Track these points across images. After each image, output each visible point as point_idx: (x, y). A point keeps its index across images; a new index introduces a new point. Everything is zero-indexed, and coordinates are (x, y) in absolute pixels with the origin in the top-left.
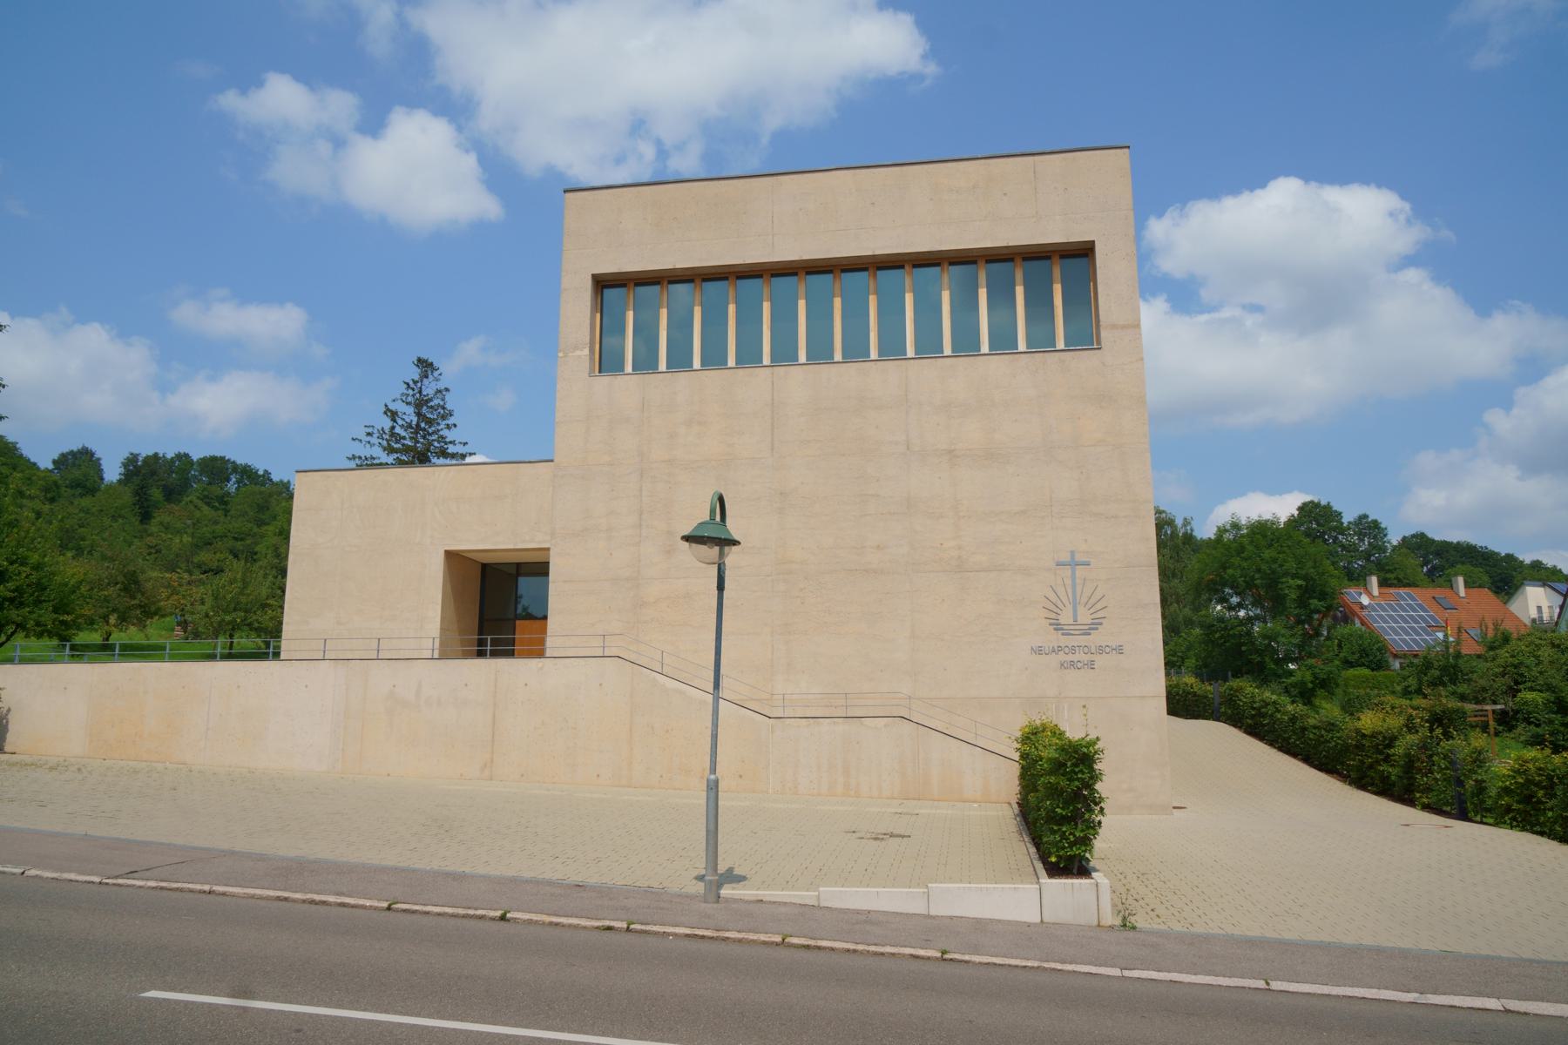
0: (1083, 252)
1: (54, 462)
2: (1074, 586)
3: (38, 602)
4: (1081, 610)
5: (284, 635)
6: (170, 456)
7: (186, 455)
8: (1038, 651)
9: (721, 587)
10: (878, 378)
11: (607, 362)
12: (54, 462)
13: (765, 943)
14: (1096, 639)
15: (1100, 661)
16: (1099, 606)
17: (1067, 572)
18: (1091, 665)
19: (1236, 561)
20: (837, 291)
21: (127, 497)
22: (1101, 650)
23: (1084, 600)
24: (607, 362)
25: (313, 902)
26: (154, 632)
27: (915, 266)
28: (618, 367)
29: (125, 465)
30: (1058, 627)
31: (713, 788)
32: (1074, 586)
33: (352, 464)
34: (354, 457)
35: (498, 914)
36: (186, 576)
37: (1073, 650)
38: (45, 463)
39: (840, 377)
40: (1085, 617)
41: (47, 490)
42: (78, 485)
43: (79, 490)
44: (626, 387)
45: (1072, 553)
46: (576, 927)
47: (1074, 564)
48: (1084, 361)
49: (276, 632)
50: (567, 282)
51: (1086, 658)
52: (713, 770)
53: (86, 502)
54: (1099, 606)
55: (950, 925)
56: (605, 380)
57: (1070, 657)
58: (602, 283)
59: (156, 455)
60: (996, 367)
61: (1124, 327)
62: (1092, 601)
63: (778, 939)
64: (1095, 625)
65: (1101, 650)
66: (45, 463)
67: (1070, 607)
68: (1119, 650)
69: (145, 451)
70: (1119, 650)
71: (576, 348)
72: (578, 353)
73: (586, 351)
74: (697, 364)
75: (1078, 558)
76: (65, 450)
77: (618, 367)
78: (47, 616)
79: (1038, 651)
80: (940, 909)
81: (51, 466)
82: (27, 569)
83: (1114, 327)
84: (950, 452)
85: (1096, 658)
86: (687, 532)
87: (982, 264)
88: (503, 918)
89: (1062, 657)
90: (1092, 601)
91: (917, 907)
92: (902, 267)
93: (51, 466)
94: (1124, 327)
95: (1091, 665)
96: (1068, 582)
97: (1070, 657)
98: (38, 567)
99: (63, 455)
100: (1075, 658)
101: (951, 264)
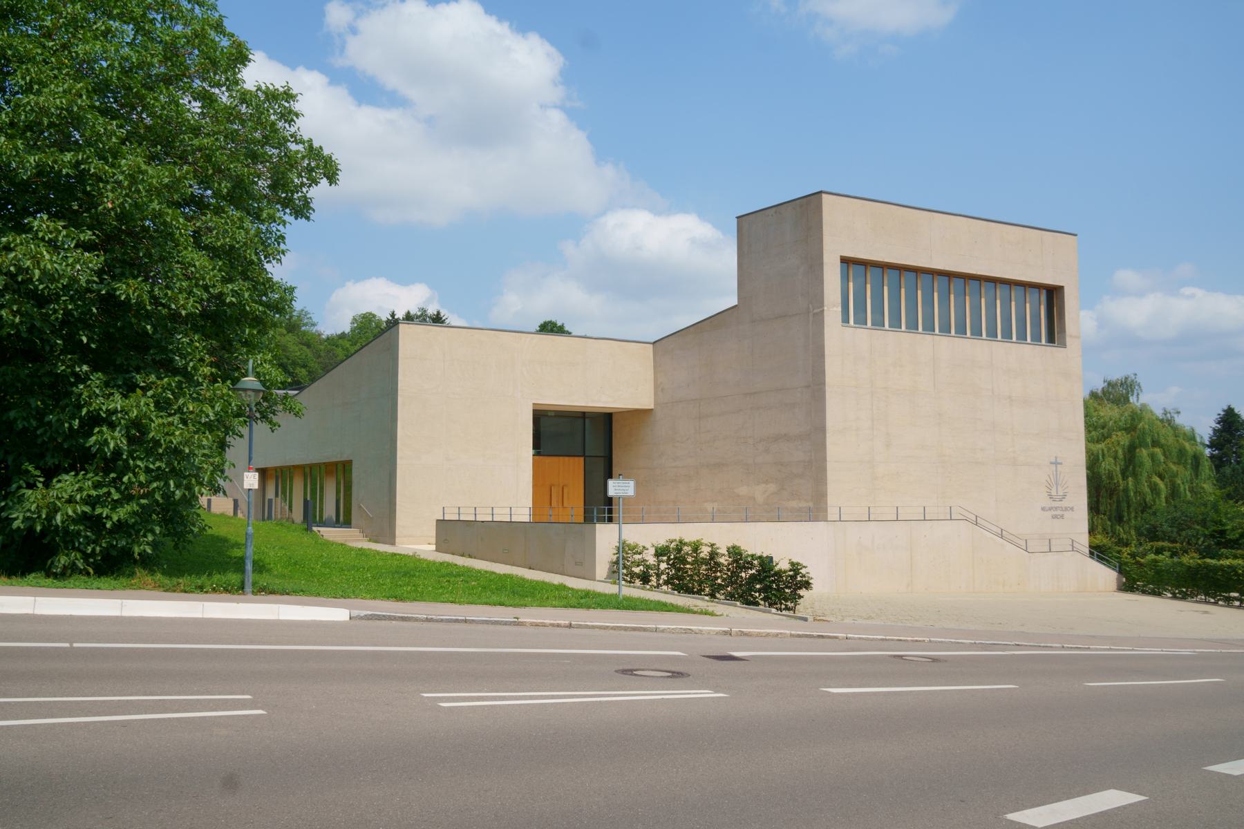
8: (1043, 509)
15: (1067, 514)
17: (1053, 467)
18: (1062, 517)
22: (1066, 509)
30: (1051, 497)
37: (1056, 508)
47: (1056, 463)
49: (816, 468)
58: (1053, 294)
65: (1066, 509)
68: (1072, 509)
70: (1072, 509)
79: (1043, 509)
84: (1010, 397)
95: (1062, 517)
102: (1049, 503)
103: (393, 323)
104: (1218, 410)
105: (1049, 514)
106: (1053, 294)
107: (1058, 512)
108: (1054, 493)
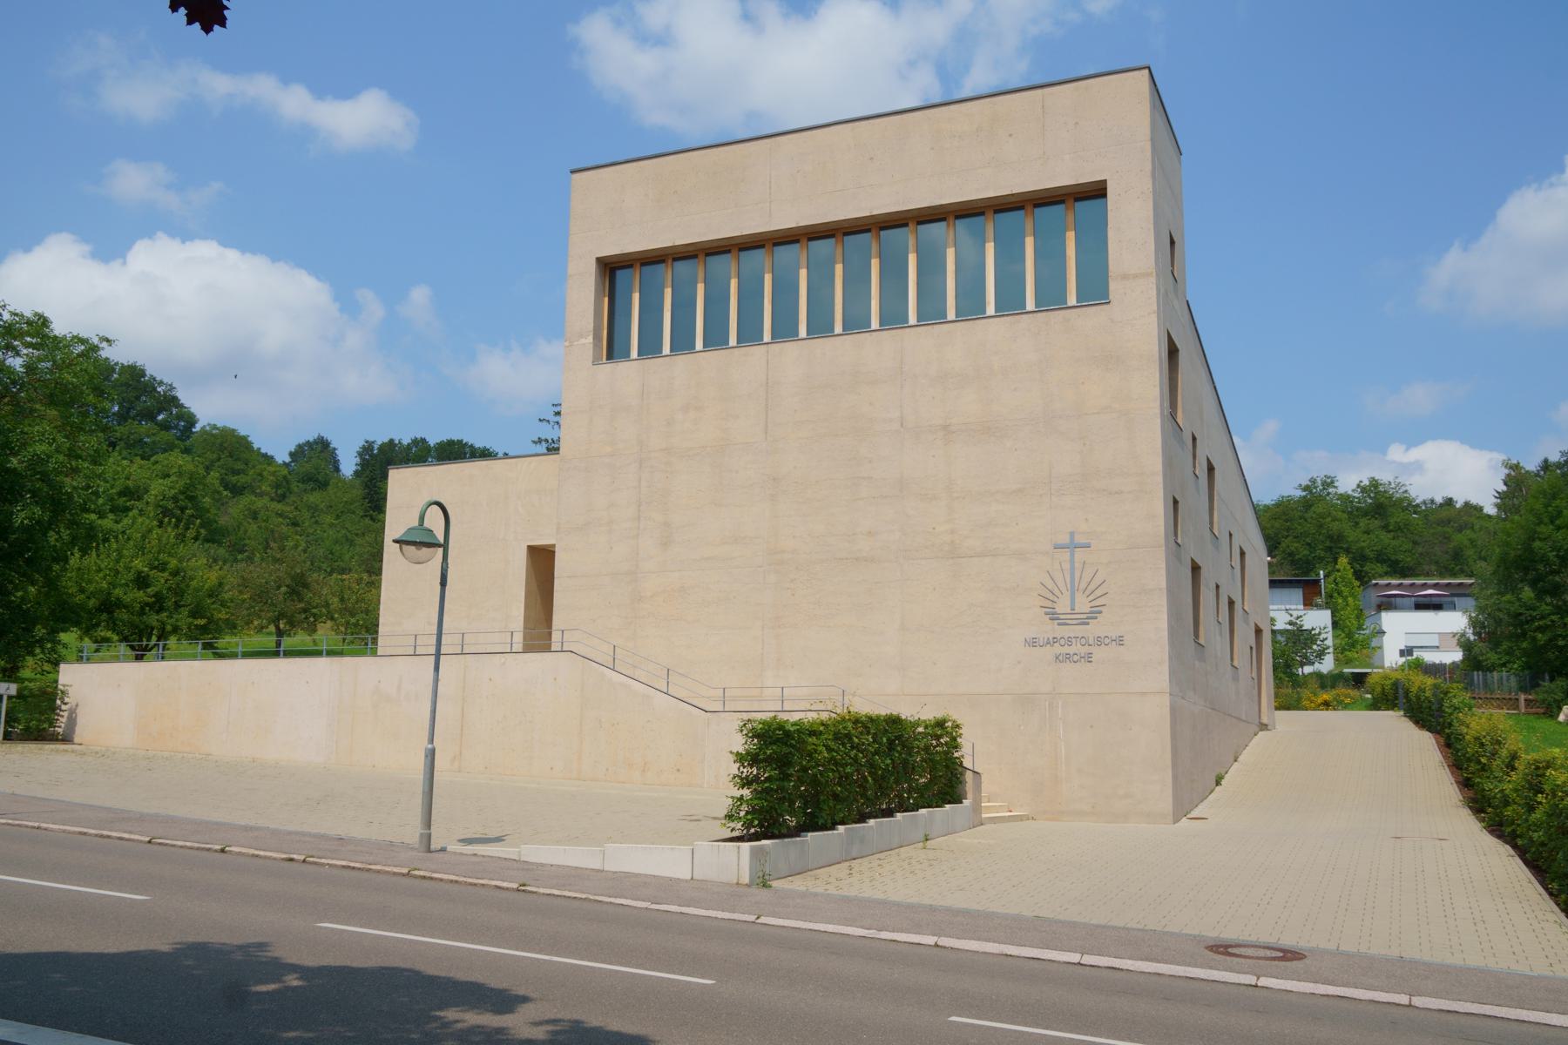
0: (1097, 192)
1: (291, 454)
2: (1073, 568)
3: (177, 606)
4: (1080, 598)
5: (381, 629)
6: (406, 442)
7: (423, 440)
8: (1032, 643)
9: (443, 583)
10: (875, 349)
11: (613, 349)
12: (291, 454)
13: (395, 874)
14: (1093, 629)
15: (1099, 653)
16: (1098, 593)
17: (1065, 555)
18: (1088, 658)
19: (1545, 530)
20: (839, 257)
21: (358, 492)
22: (1100, 641)
23: (1083, 585)
24: (613, 349)
25: (102, 836)
26: (325, 633)
27: (996, 212)
28: (626, 355)
29: (360, 454)
30: (1053, 616)
31: (431, 755)
32: (1073, 568)
33: (542, 448)
34: (540, 441)
35: (218, 847)
36: (365, 576)
37: (1070, 641)
38: (282, 456)
39: (840, 350)
40: (1083, 605)
41: (277, 486)
42: (310, 479)
43: (312, 485)
44: (629, 373)
45: (1072, 534)
46: (269, 858)
47: (1073, 546)
48: (1093, 318)
49: (372, 628)
50: (572, 268)
51: (1084, 650)
52: (431, 741)
53: (314, 498)
54: (1098, 593)
55: (526, 866)
56: (608, 368)
57: (1067, 650)
58: (611, 269)
59: (391, 441)
60: (994, 331)
61: (1136, 276)
62: (1092, 587)
63: (405, 871)
64: (1094, 614)
65: (1100, 641)
66: (282, 456)
67: (1067, 594)
68: (1120, 641)
69: (380, 439)
70: (1120, 641)
71: (581, 336)
72: (583, 341)
73: (590, 339)
74: (803, 332)
75: (1079, 539)
76: (302, 441)
77: (626, 355)
78: (183, 618)
79: (1032, 643)
80: (611, 866)
81: (288, 459)
82: (166, 574)
83: (1125, 277)
85: (1091, 649)
86: (397, 537)
87: (990, 214)
88: (223, 851)
89: (1057, 649)
90: (1092, 587)
91: (595, 864)
92: (906, 225)
93: (288, 459)
94: (1136, 276)
95: (1088, 658)
96: (1066, 566)
97: (1067, 650)
98: (175, 573)
99: (300, 446)
100: (1071, 650)
101: (957, 217)
102: (1051, 629)
103: (380, 461)
104: (594, 262)
105: (1049, 652)
106: (611, 269)
107: (1076, 648)
108: (1063, 606)
